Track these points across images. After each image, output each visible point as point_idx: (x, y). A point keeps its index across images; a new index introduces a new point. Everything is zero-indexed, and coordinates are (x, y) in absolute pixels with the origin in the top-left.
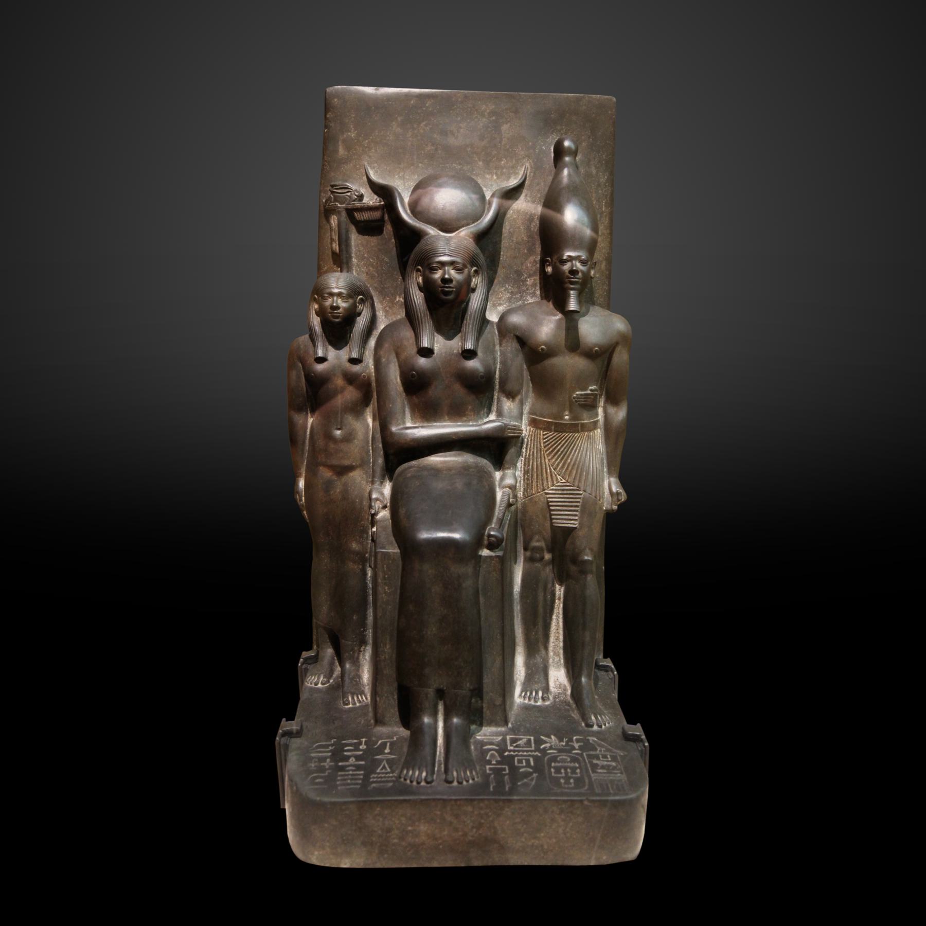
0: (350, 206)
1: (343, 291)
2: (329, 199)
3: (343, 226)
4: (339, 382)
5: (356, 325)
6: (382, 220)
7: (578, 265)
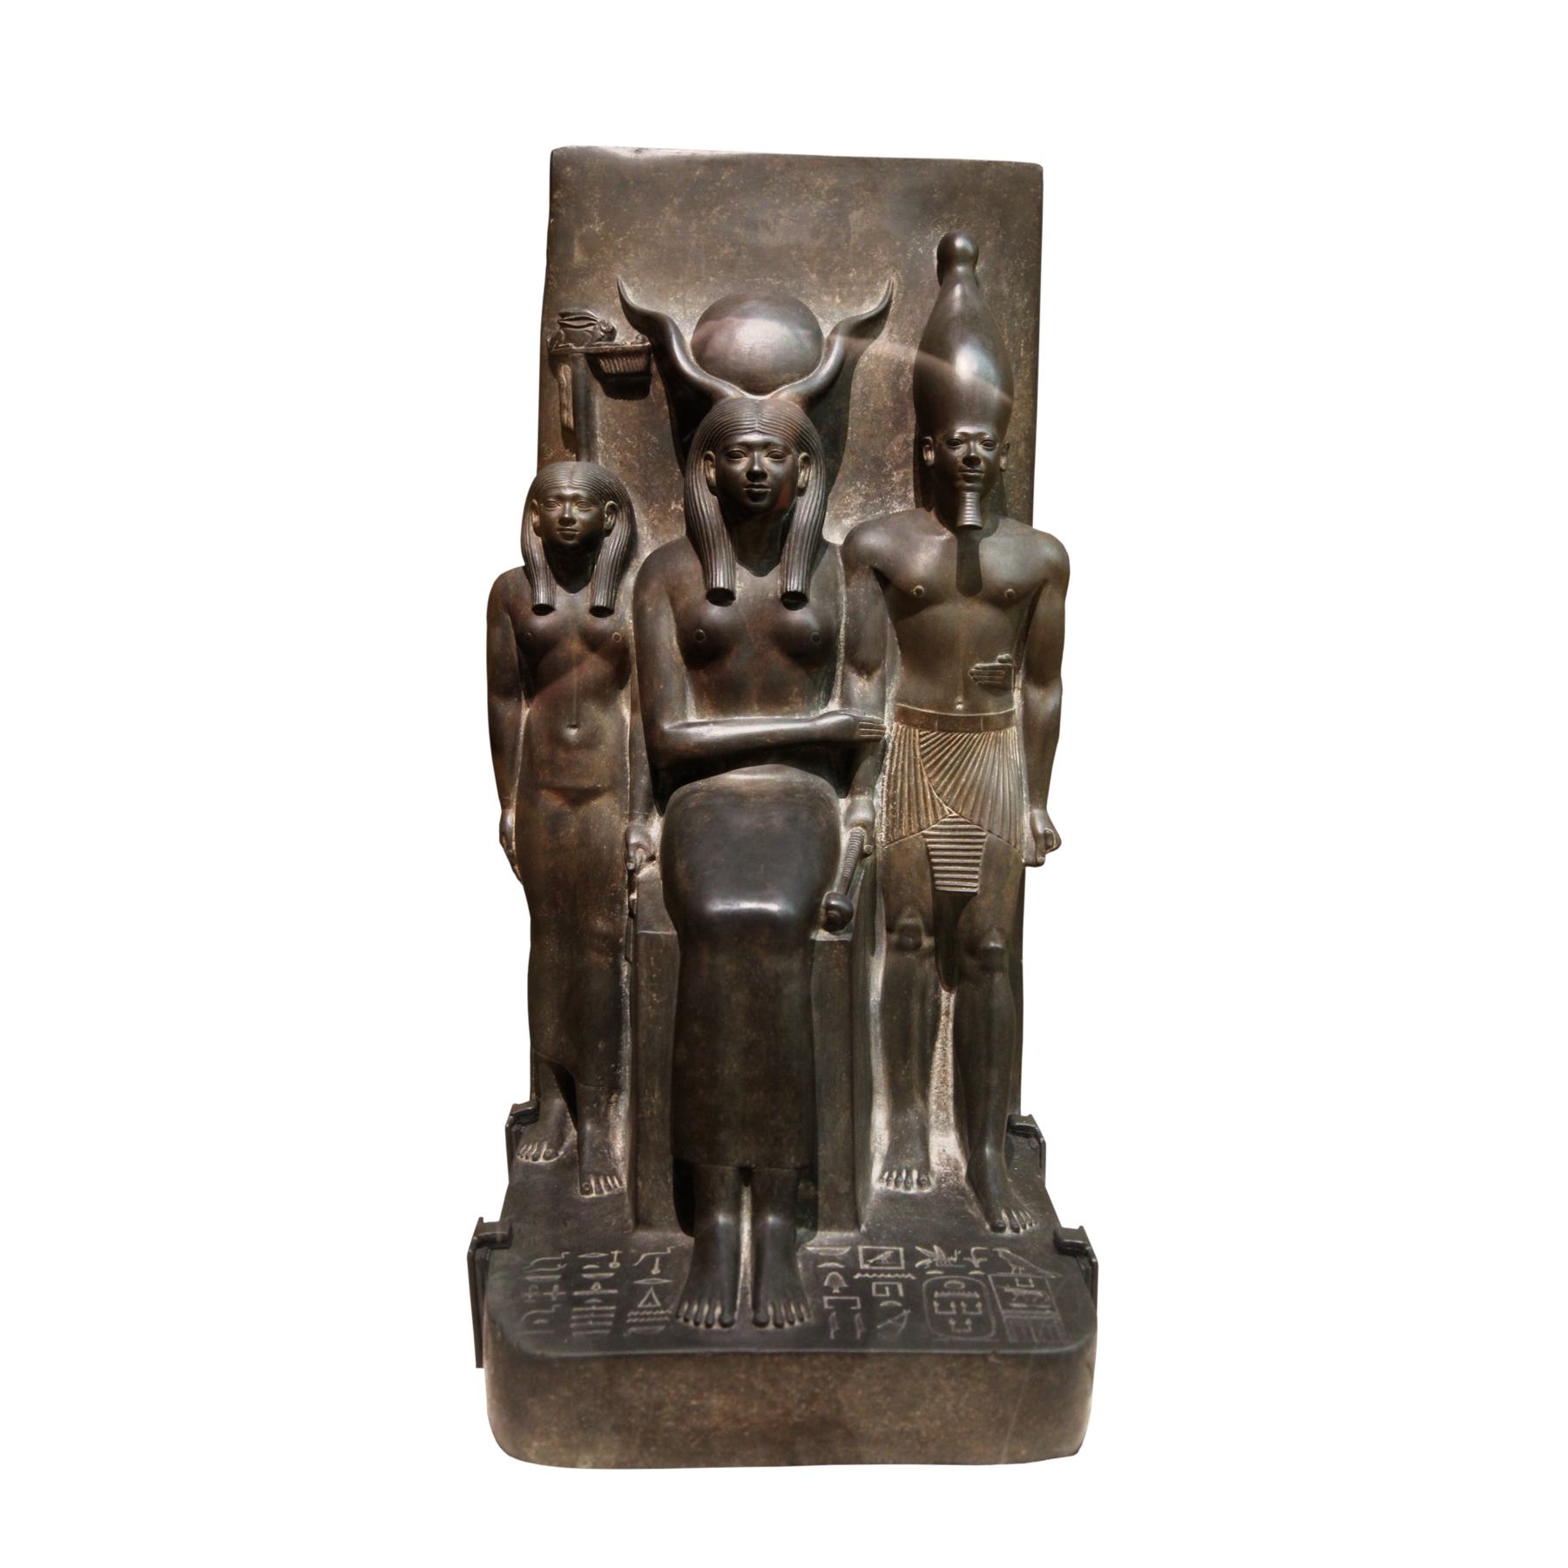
0: (592, 349)
1: (580, 492)
2: (556, 338)
3: (581, 383)
4: (575, 646)
5: (603, 550)
6: (646, 373)
7: (979, 449)
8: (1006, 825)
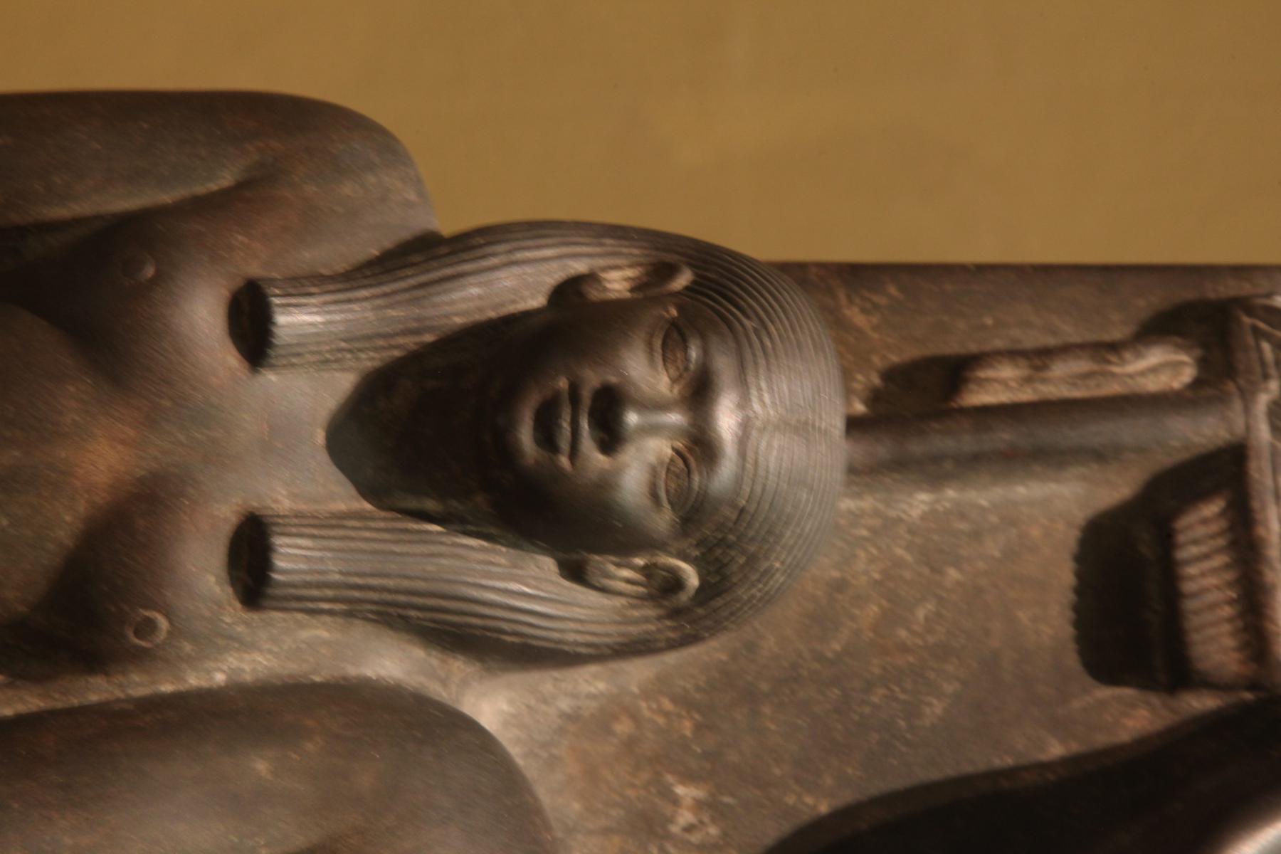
0: (1262, 473)
1: (726, 470)
3: (1128, 430)
4: (102, 456)
5: (501, 556)
6: (1176, 672)
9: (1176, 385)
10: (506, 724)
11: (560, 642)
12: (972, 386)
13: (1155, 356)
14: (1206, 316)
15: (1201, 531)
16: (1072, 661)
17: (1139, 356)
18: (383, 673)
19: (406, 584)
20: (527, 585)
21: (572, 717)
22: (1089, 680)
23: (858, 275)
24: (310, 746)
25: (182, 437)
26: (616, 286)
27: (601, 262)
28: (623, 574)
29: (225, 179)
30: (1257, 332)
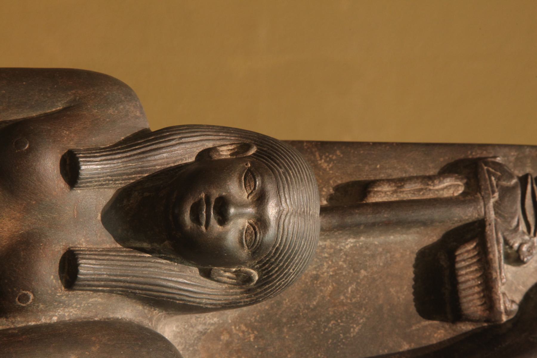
0: (491, 231)
1: (271, 232)
2: (503, 172)
3: (437, 213)
5: (176, 267)
6: (451, 311)
8: (100, 175)
9: (456, 194)
10: (175, 336)
11: (199, 303)
12: (372, 194)
13: (448, 182)
14: (470, 166)
15: (466, 256)
16: (413, 309)
17: (440, 182)
18: (124, 316)
19: (135, 279)
20: (186, 279)
21: (203, 333)
22: (419, 317)
23: (324, 146)
24: (93, 349)
25: (40, 216)
26: (225, 153)
27: (218, 143)
28: (227, 275)
29: (59, 107)
30: (488, 171)
